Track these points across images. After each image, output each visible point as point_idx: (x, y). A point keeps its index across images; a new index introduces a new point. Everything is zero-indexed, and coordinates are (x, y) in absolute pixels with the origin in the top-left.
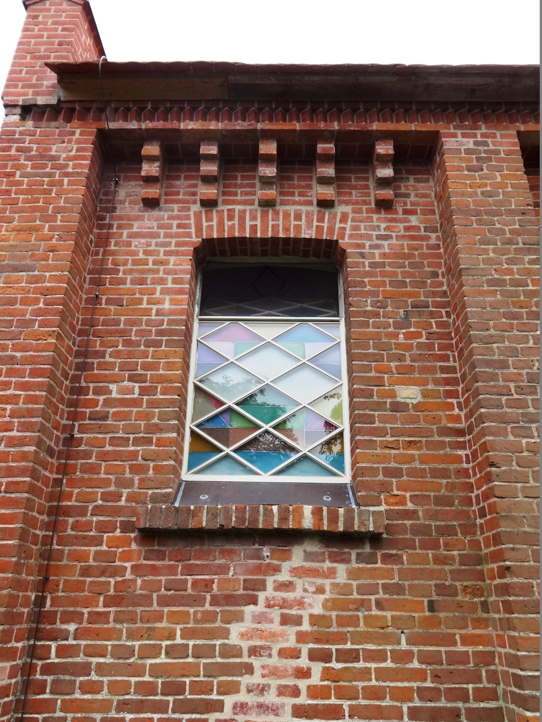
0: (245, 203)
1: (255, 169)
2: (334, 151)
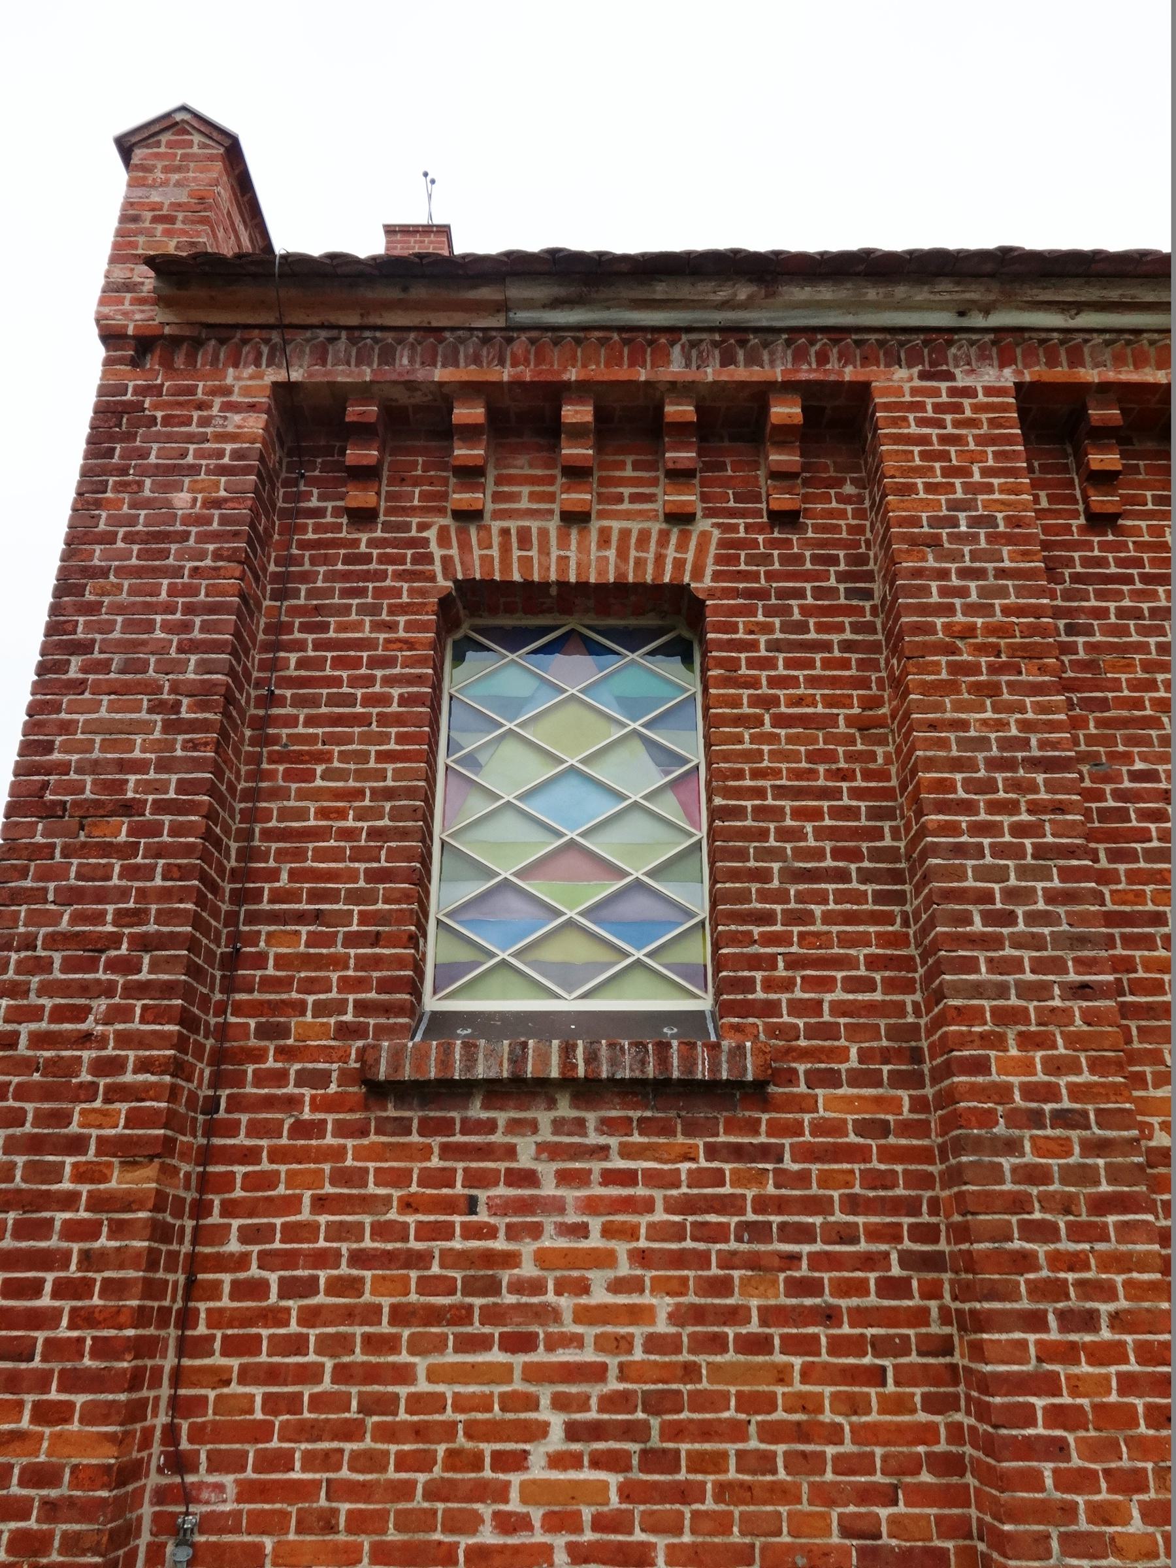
0: (628, 515)
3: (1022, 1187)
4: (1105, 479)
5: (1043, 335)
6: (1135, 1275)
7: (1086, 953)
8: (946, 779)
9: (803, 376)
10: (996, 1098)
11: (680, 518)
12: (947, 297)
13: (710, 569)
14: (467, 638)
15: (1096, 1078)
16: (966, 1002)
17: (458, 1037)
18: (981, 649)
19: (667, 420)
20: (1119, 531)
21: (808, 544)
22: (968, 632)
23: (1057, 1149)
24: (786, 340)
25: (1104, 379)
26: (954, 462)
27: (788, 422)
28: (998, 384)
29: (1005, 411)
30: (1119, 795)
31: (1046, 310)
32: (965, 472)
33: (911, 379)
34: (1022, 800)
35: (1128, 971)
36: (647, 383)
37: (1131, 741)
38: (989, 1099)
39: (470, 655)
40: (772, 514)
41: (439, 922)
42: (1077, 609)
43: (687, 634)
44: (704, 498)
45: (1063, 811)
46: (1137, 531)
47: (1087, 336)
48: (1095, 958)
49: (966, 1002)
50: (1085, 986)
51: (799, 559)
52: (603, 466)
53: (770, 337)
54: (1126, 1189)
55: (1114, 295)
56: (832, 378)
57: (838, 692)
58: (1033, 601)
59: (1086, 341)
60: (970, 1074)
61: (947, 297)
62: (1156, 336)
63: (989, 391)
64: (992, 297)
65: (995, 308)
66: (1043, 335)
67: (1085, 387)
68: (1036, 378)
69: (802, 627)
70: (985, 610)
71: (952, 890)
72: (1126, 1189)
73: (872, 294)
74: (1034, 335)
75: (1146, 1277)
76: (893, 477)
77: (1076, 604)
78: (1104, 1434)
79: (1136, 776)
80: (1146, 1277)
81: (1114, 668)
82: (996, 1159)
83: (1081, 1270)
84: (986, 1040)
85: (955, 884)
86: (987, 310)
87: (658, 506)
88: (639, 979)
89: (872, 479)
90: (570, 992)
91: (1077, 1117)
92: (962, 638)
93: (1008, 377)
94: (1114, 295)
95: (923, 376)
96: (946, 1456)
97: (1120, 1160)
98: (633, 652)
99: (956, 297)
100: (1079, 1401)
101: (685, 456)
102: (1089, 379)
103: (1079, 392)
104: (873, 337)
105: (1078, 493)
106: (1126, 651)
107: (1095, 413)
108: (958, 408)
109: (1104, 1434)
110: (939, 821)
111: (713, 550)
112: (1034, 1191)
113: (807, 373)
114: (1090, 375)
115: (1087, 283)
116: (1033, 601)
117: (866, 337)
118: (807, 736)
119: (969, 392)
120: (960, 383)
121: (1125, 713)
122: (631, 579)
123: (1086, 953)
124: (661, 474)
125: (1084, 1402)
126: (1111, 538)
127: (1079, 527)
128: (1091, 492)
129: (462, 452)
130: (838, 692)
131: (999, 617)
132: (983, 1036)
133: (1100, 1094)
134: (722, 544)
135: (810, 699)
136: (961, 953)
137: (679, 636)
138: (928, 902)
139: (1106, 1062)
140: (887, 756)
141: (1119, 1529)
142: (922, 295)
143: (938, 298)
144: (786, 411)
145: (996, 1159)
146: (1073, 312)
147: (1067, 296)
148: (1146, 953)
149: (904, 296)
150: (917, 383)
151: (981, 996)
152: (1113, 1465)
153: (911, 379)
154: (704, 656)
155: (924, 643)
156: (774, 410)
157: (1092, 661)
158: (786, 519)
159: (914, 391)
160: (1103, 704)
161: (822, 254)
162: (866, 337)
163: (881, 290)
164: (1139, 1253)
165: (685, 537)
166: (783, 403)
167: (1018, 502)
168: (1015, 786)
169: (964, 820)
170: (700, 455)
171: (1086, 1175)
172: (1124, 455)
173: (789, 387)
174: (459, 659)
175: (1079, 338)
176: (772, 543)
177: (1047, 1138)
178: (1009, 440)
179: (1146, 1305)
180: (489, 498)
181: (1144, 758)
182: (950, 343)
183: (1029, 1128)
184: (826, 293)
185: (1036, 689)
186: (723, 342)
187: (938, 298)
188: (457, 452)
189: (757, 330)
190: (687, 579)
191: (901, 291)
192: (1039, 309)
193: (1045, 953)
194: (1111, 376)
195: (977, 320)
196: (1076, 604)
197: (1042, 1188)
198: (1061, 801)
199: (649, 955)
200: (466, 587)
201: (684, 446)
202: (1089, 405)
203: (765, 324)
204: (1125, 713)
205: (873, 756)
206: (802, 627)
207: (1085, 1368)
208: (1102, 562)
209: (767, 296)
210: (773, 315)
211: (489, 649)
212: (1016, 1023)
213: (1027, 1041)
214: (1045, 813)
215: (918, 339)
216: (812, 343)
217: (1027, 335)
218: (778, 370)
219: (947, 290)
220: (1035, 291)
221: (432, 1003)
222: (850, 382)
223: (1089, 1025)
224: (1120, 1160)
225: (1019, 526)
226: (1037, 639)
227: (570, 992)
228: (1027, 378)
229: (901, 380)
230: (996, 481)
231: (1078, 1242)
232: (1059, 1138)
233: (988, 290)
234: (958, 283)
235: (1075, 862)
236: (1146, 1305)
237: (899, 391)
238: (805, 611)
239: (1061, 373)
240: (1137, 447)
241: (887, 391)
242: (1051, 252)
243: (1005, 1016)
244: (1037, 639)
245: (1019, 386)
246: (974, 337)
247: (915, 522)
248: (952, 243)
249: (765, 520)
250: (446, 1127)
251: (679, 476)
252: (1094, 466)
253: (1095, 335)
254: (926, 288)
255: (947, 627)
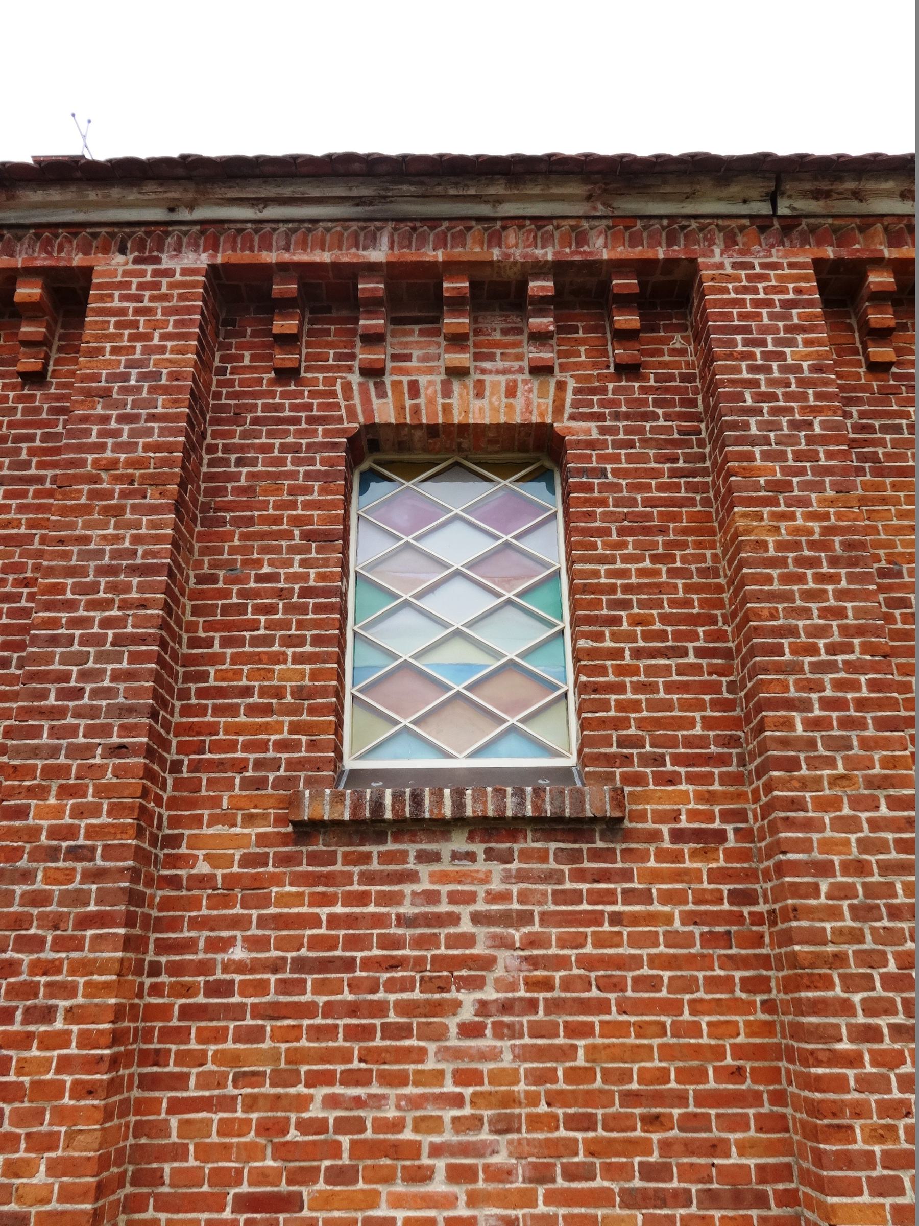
1: (437, 320)
2: (637, 290)
3: (26, 909)
4: (288, 341)
5: (239, 226)
6: (95, 977)
7: (131, 720)
8: (58, 584)
9: (39, 263)
10: (26, 838)
11: (541, 370)
12: (153, 196)
13: (568, 410)
14: (371, 470)
15: (110, 820)
16: (23, 762)
17: (370, 787)
18: (118, 479)
19: (446, 294)
20: (300, 382)
21: (48, 398)
22: (113, 464)
23: (61, 877)
24: (35, 234)
25: (280, 260)
26: (141, 329)
27: (28, 300)
28: (193, 266)
29: (194, 287)
30: (242, 594)
31: (239, 205)
32: (147, 337)
33: (127, 263)
34: (117, 599)
35: (211, 734)
36: (667, 261)
37: (264, 550)
38: (20, 839)
39: (373, 485)
40: (618, 367)
41: (354, 697)
42: (248, 446)
43: (548, 464)
44: (560, 354)
45: (144, 607)
46: (315, 382)
47: (274, 226)
48: (136, 724)
49: (23, 762)
50: (122, 746)
51: (38, 410)
52: (477, 332)
53: (20, 232)
54: (108, 908)
55: (287, 192)
56: (62, 264)
57: (40, 516)
58: (171, 439)
59: (274, 230)
60: (10, 819)
61: (153, 196)
62: (330, 224)
63: (185, 272)
64: (190, 195)
65: (198, 205)
66: (239, 226)
67: (266, 269)
68: (226, 260)
69: (26, 465)
70: (129, 447)
71: (38, 672)
72: (108, 908)
73: (93, 195)
74: (232, 226)
75: (103, 978)
76: (88, 342)
77: (249, 441)
78: (34, 1105)
79: (260, 578)
80: (103, 978)
81: (266, 492)
82: (11, 887)
83: (53, 974)
84: (31, 792)
85: (43, 668)
86: (191, 207)
87: (441, 364)
88: (512, 742)
89: (700, 335)
90: (460, 752)
91: (85, 851)
92: (106, 470)
93: (203, 260)
94: (287, 192)
95: (136, 261)
96: (771, 1115)
97: (110, 885)
98: (505, 479)
99: (161, 196)
100: (21, 1079)
101: (627, 320)
102: (269, 260)
103: (266, 272)
104: (103, 230)
105: (859, 345)
106: (278, 478)
107: (278, 288)
108: (156, 286)
109: (34, 1105)
110: (43, 617)
111: (569, 397)
112: (35, 911)
113: (42, 261)
114: (270, 257)
115: (265, 182)
116: (171, 439)
117: (98, 230)
118: (6, 552)
119: (169, 273)
120: (163, 266)
121: (265, 528)
122: (440, 421)
123: (131, 720)
124: (524, 337)
125: (26, 1079)
126: (293, 387)
127: (269, 380)
128: (870, 343)
129: (284, 325)
130: (40, 516)
131: (140, 453)
132: (29, 789)
133: (109, 833)
134: (577, 391)
135: (15, 523)
136: (30, 722)
137: (542, 467)
138: (753, 674)
139: (123, 807)
140: (715, 557)
141: (24, 1180)
142: (132, 195)
143: (146, 197)
144: (540, 286)
145: (11, 887)
146: (261, 206)
147: (250, 193)
148: (229, 719)
149: (117, 196)
150: (131, 266)
151: (36, 756)
152: (34, 1130)
153: (127, 263)
154: (565, 480)
155: (74, 475)
156: (18, 291)
157: (250, 487)
158: (36, 379)
159: (126, 273)
160: (250, 521)
161: (110, 161)
162: (98, 230)
163: (99, 192)
164: (102, 959)
165: (381, 387)
166: (26, 285)
167: (183, 360)
168: (113, 588)
169: (64, 616)
170: (557, 320)
171: (80, 898)
172: (896, 315)
173: (30, 272)
174: (363, 490)
175: (268, 227)
176: (19, 399)
177: (57, 869)
178: (810, 303)
179: (96, 1001)
180: (388, 358)
181: (271, 563)
182: (167, 234)
183: (45, 861)
184: (55, 195)
185: (153, 509)
186: (614, 227)
187: (146, 197)
188: (23, 329)
189: (10, 227)
190: (549, 420)
191: (116, 193)
192: (233, 205)
193: (98, 721)
194: (287, 257)
195: (184, 215)
196: (249, 441)
197: (41, 909)
198: (146, 599)
199: (415, 722)
200: (370, 428)
201: (461, 314)
202: (275, 281)
203: (13, 221)
204: (265, 528)
205: (703, 558)
206: (26, 465)
207: (35, 1052)
208: (279, 408)
209: (8, 199)
210: (21, 214)
211: (390, 480)
212: (58, 778)
213: (66, 792)
214: (130, 609)
215: (140, 232)
216: (56, 236)
217: (226, 226)
218: (20, 260)
219: (151, 190)
220: (225, 190)
221: (350, 763)
222: (78, 267)
223: (118, 777)
224: (110, 885)
225: (177, 379)
226: (166, 470)
227: (460, 752)
228: (219, 260)
229: (118, 264)
230: (169, 344)
231: (58, 951)
232: (67, 869)
233: (186, 190)
234: (161, 185)
235: (144, 648)
236: (96, 1001)
237: (114, 274)
238: (32, 452)
239: (244, 257)
240: (334, 315)
241: (103, 274)
242: (221, 158)
243: (51, 772)
244: (166, 470)
245: (212, 267)
246: (184, 228)
247: (96, 378)
248: (143, 153)
249: (612, 370)
250: (435, 857)
251: (540, 338)
252: (873, 325)
253: (281, 225)
254: (135, 190)
255: (96, 462)
